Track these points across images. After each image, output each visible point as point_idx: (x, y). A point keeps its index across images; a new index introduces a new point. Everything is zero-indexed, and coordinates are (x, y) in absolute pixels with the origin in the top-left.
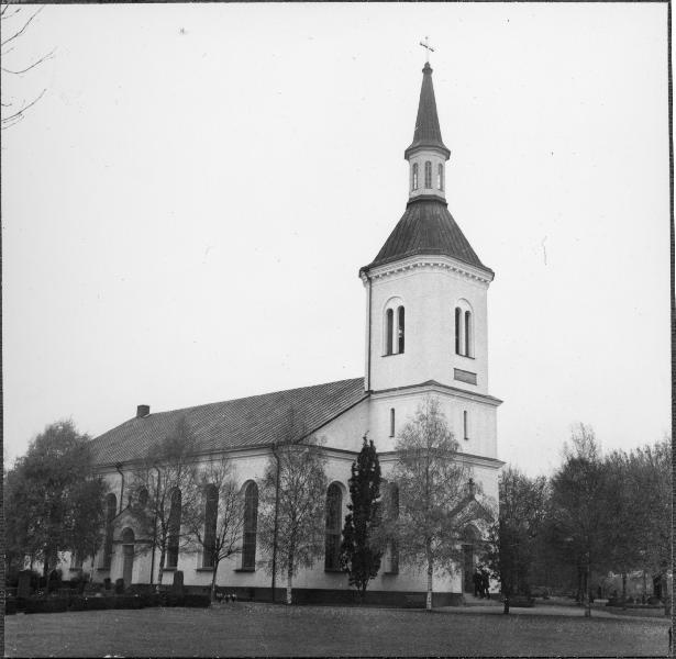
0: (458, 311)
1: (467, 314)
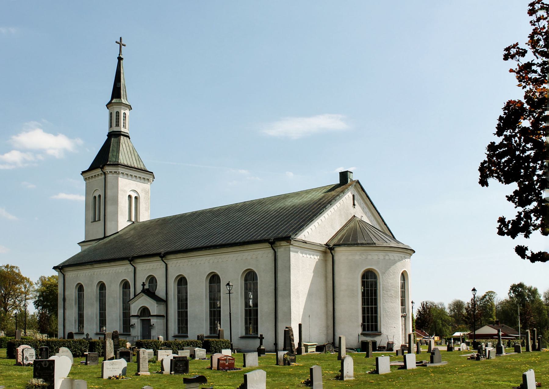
0: (130, 197)
1: (136, 198)
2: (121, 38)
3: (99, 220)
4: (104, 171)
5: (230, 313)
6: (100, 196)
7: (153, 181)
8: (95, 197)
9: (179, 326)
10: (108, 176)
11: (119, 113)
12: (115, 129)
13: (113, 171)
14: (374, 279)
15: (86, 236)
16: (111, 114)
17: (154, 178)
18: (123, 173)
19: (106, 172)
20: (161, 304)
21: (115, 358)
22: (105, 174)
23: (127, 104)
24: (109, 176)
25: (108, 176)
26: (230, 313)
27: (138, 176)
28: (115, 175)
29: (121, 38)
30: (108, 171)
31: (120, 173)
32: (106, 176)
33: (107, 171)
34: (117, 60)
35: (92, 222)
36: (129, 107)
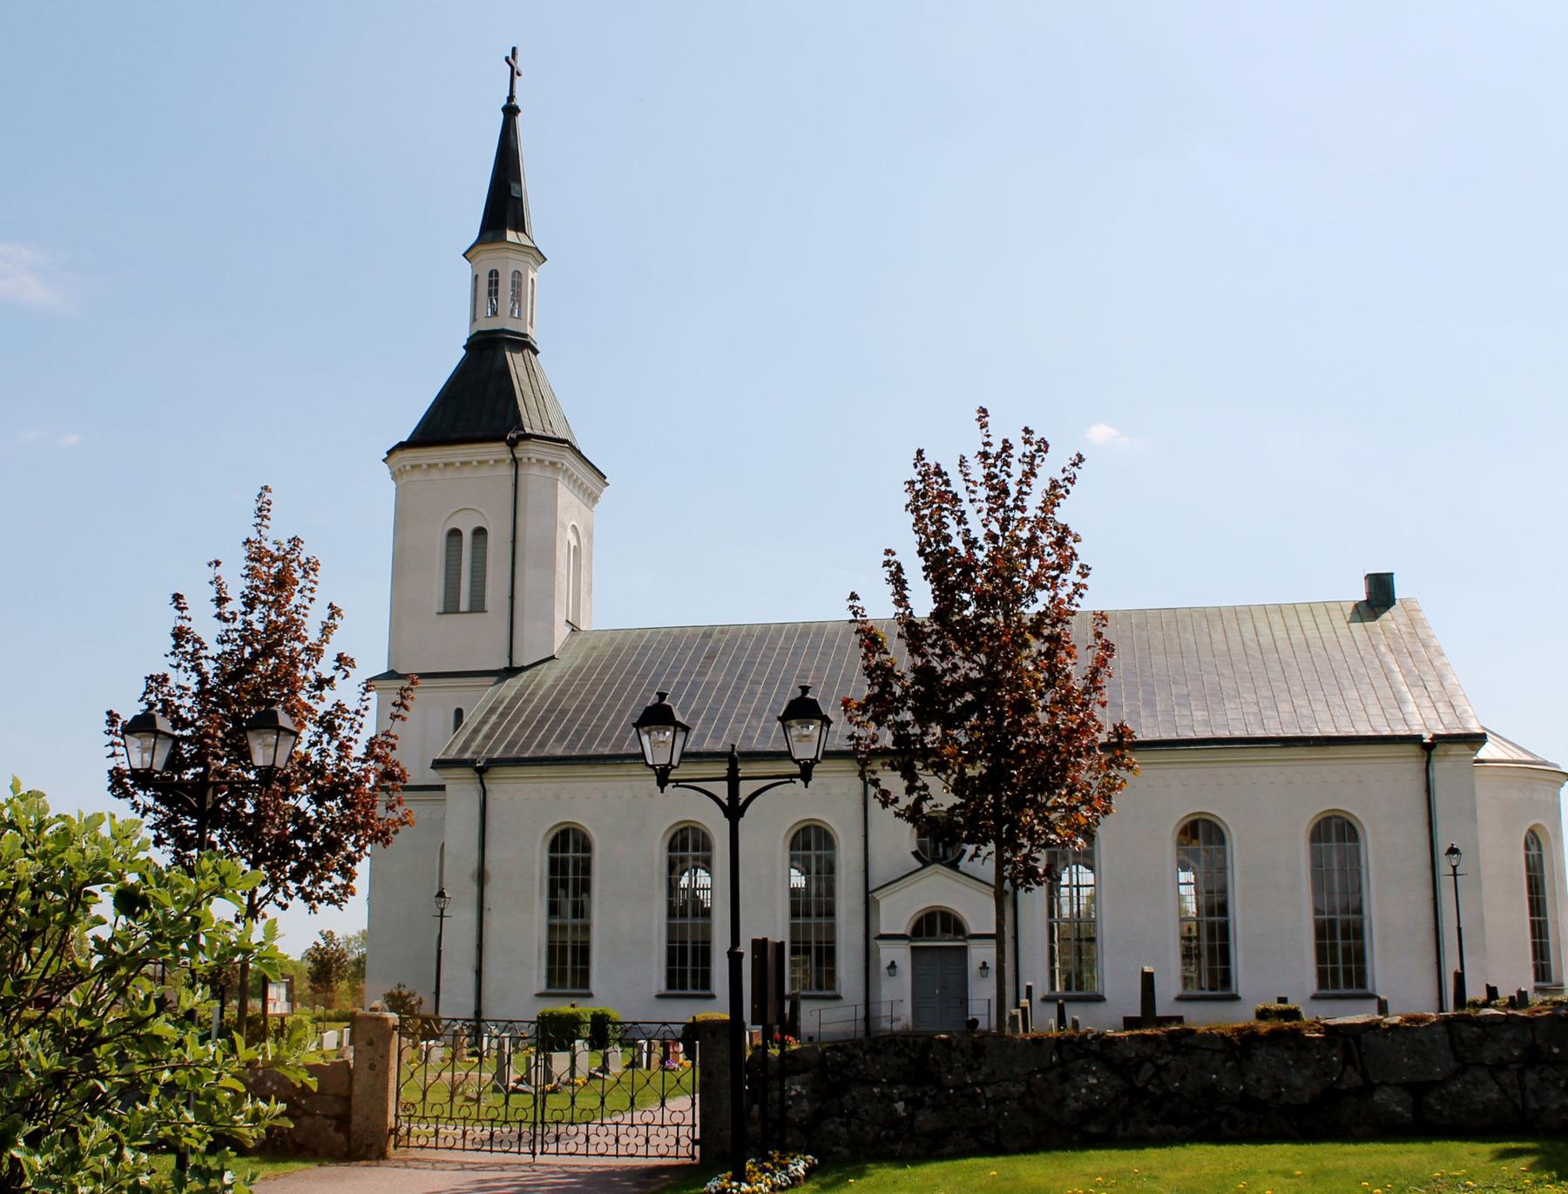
2: (514, 49)
3: (478, 606)
4: (517, 455)
5: (1459, 929)
6: (480, 532)
7: (967, 488)
8: (455, 534)
9: (1359, 942)
10: (530, 472)
11: (497, 274)
12: (505, 322)
13: (548, 459)
14: (1219, 915)
15: (392, 655)
16: (476, 278)
17: (605, 477)
18: (540, 461)
19: (525, 460)
20: (950, 878)
21: (1540, 984)
22: (516, 462)
23: (523, 243)
24: (531, 474)
25: (530, 472)
26: (1459, 929)
27: (424, 462)
28: (548, 473)
29: (514, 49)
30: (534, 456)
31: (533, 460)
32: (521, 471)
33: (531, 455)
34: (501, 116)
35: (439, 613)
36: (534, 252)
